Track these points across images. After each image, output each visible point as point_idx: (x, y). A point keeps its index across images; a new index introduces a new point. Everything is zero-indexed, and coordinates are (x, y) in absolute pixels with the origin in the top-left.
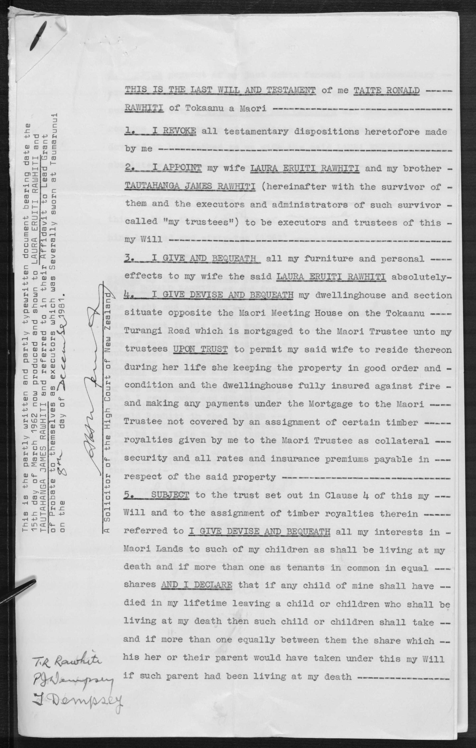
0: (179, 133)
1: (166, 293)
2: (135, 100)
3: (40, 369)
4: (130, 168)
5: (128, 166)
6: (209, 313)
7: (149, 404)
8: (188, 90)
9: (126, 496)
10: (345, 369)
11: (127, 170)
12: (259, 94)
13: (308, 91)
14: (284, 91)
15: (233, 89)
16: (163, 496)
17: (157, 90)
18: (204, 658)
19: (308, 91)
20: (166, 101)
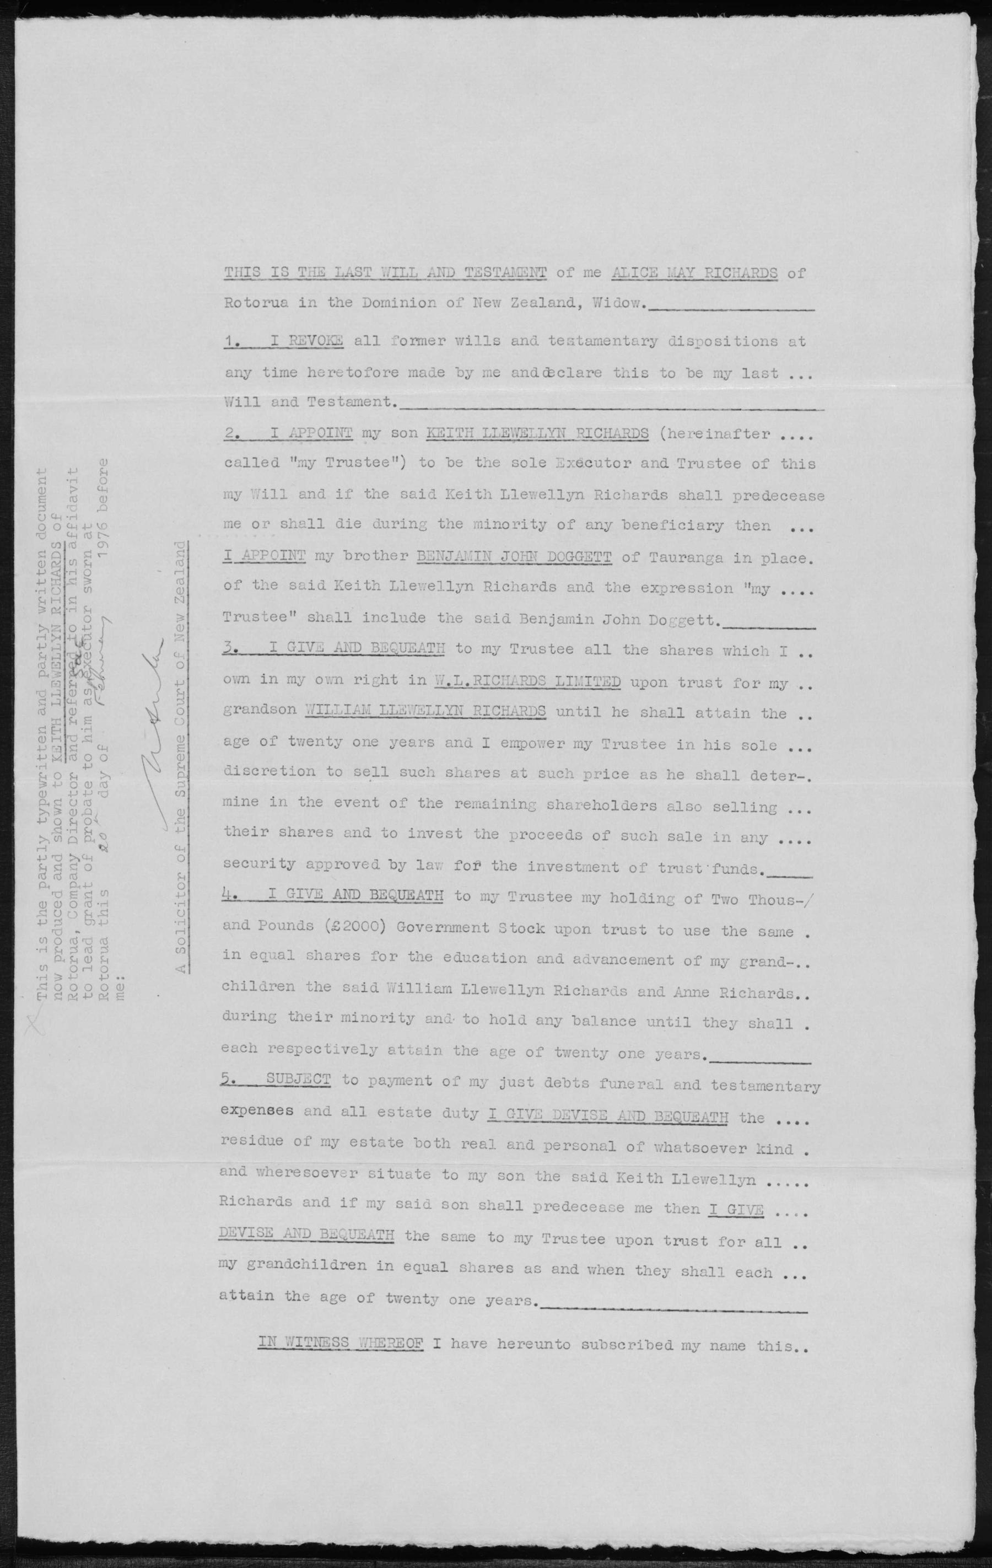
0: (316, 344)
2: (239, 290)
3: (66, 808)
4: (234, 435)
5: (230, 430)
6: (543, 464)
7: (292, 374)
8: (331, 273)
9: (224, 1080)
10: (412, 866)
11: (228, 439)
12: (451, 278)
13: (539, 275)
14: (494, 274)
15: (407, 271)
16: (285, 1080)
17: (279, 272)
18: (259, 833)
19: (539, 275)
20: (292, 291)
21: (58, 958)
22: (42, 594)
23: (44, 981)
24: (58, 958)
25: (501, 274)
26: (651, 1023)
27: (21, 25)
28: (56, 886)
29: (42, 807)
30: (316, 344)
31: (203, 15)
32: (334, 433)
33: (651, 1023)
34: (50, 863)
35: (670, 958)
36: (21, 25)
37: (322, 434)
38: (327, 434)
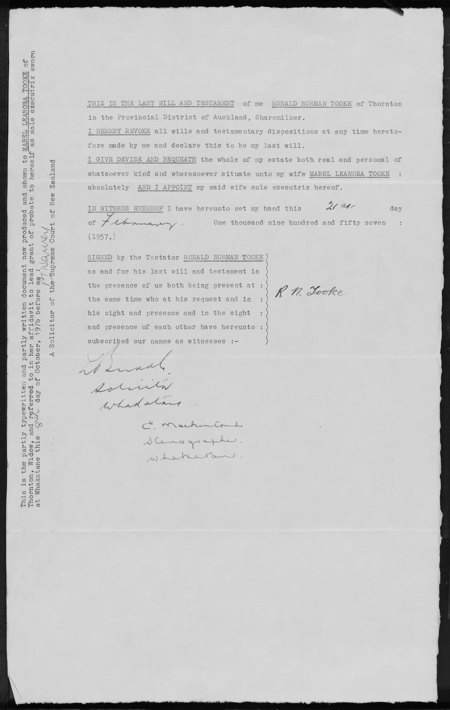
0: (137, 133)
1: (98, 158)
14: (210, 104)
21: (31, 387)
22: (24, 322)
23: (24, 498)
24: (31, 387)
25: (213, 104)
26: (258, 174)
27: (13, 13)
28: (30, 358)
29: (24, 419)
30: (137, 133)
31: (441, 575)
32: (183, 187)
33: (258, 174)
34: (27, 348)
35: (194, 116)
36: (13, 13)
37: (178, 188)
38: (180, 188)
